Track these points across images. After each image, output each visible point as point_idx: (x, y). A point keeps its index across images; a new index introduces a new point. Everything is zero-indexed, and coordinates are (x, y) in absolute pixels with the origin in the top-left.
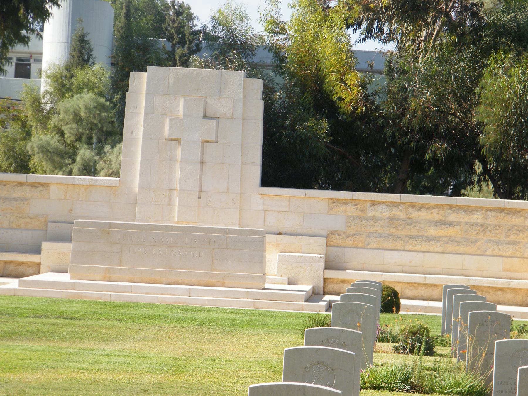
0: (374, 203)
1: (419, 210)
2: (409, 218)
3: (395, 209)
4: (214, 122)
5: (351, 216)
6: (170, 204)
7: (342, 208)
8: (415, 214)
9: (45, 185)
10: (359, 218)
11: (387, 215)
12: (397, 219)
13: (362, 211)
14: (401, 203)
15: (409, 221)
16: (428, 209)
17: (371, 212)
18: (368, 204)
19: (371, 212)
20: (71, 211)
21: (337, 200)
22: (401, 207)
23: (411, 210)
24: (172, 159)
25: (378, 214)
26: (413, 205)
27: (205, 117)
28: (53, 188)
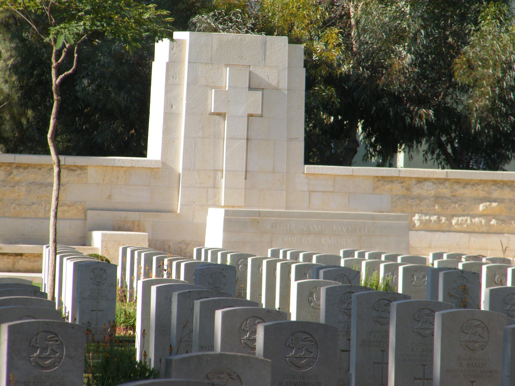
0: (420, 181)
1: (464, 187)
2: (454, 196)
3: (441, 186)
4: (260, 93)
5: (397, 195)
6: (215, 186)
7: (388, 186)
8: (461, 191)
9: (82, 168)
10: (404, 197)
11: (433, 193)
12: (442, 197)
13: (408, 189)
14: (446, 180)
15: (454, 199)
16: (473, 185)
17: (416, 191)
18: (414, 182)
19: (416, 191)
20: (110, 197)
21: (383, 177)
22: (447, 184)
23: (456, 187)
24: (217, 137)
25: (424, 193)
26: (457, 182)
27: (250, 88)
28: (91, 171)
